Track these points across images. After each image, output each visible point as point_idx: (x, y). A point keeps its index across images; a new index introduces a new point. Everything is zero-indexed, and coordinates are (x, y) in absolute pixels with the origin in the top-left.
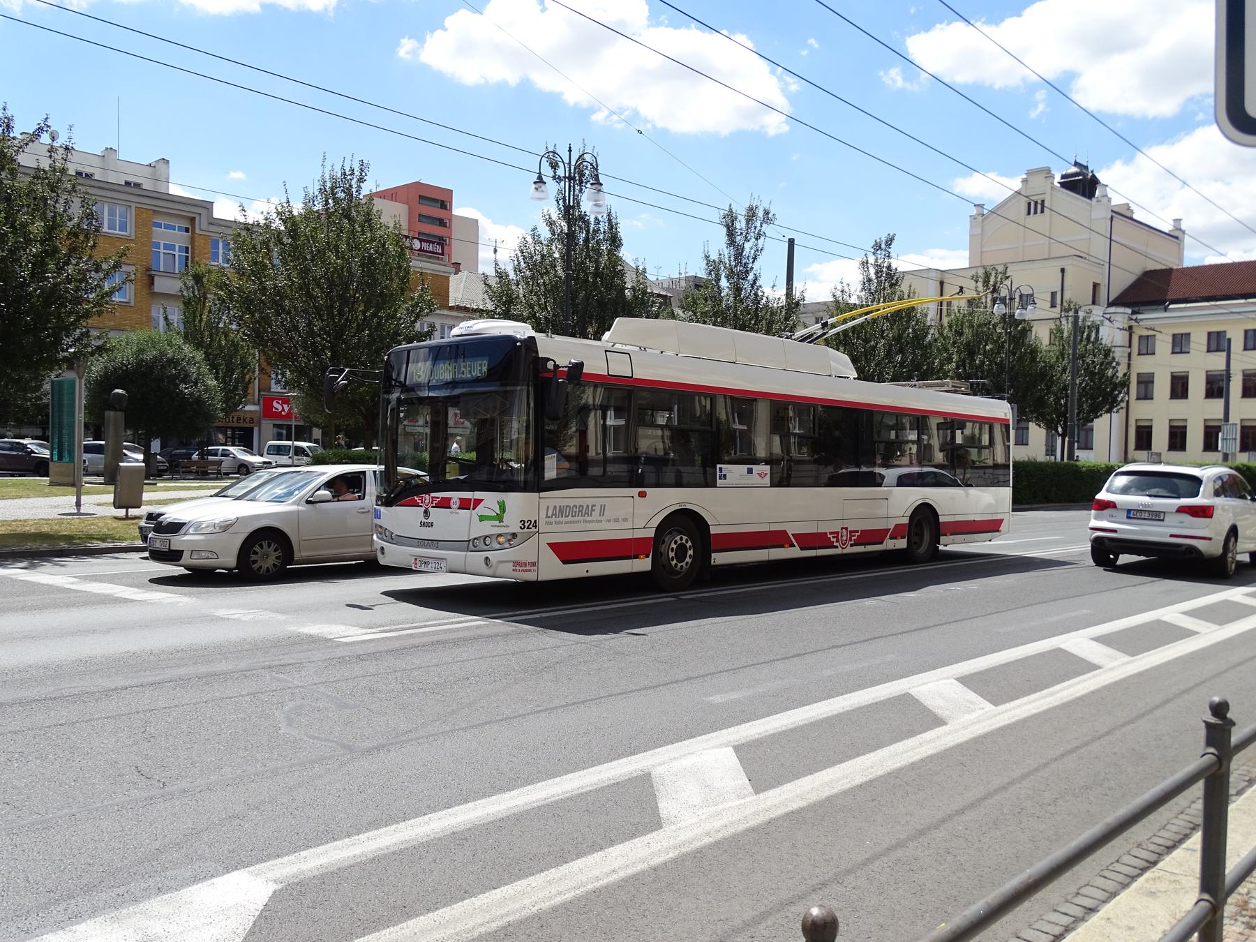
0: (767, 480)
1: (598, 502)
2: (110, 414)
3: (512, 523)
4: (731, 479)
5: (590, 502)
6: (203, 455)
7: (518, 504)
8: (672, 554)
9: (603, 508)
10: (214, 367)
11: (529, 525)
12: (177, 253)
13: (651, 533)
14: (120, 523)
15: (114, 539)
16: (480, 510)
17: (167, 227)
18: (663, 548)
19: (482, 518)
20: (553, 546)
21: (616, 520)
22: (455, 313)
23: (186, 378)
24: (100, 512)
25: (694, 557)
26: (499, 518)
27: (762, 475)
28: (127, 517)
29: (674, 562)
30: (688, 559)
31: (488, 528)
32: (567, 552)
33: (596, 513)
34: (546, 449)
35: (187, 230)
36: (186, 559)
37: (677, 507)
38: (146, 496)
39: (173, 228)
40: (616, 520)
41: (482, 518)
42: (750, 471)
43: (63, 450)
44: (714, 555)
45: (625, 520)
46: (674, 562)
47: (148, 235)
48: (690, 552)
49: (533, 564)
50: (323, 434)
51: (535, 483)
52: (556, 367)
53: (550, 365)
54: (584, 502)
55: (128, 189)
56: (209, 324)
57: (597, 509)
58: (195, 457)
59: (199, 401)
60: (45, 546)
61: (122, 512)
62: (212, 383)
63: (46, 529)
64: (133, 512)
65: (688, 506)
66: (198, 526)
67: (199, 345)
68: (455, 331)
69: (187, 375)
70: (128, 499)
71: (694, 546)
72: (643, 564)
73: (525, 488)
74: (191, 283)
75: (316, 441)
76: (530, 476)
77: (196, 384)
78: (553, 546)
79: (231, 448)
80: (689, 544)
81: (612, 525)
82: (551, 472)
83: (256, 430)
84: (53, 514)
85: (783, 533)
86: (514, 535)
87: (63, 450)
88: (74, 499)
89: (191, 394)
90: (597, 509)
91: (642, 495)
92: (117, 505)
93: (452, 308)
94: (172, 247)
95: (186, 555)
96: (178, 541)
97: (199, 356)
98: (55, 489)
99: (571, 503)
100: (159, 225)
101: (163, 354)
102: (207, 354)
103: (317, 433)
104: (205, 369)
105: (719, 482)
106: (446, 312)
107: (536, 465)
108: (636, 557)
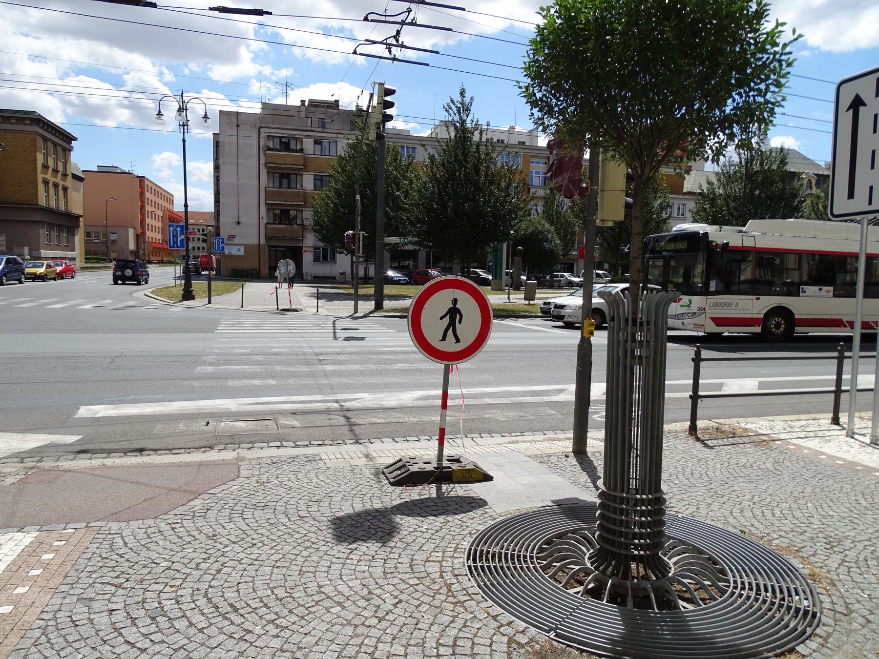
0: (831, 294)
1: (735, 301)
2: (516, 258)
3: (694, 308)
4: (808, 293)
5: (731, 301)
6: (552, 277)
7: (697, 301)
8: (772, 326)
9: (737, 304)
10: (559, 234)
11: (702, 310)
12: (541, 176)
13: (762, 316)
14: (526, 307)
15: (531, 313)
16: (681, 303)
17: (537, 163)
18: (768, 323)
19: (681, 306)
20: (712, 319)
21: (744, 309)
22: (687, 197)
23: (546, 240)
24: (518, 302)
25: (785, 329)
26: (689, 306)
27: (828, 292)
28: (529, 304)
29: (773, 330)
30: (781, 329)
31: (684, 310)
32: (719, 322)
33: (733, 307)
34: (711, 276)
35: (546, 163)
36: (566, 319)
37: (776, 305)
38: (537, 296)
39: (539, 163)
40: (744, 309)
41: (681, 306)
42: (820, 289)
43: (497, 275)
44: (796, 328)
45: (748, 309)
46: (773, 330)
47: (528, 168)
48: (783, 326)
49: (703, 325)
50: (610, 266)
51: (705, 292)
52: (717, 244)
53: (714, 244)
54: (728, 301)
55: (519, 146)
56: (557, 211)
57: (734, 304)
58: (548, 278)
59: (552, 251)
60: (505, 313)
61: (527, 302)
62: (558, 242)
63: (501, 307)
64: (531, 302)
65: (783, 305)
66: (570, 307)
67: (551, 224)
68: (674, 229)
69: (547, 239)
70: (530, 297)
71: (785, 323)
72: (758, 329)
73: (700, 294)
74: (549, 191)
75: (606, 270)
76: (703, 290)
77: (551, 242)
78: (712, 319)
79: (565, 274)
80: (783, 322)
81: (741, 311)
82: (712, 288)
83: (575, 264)
84: (501, 302)
85: (841, 320)
86: (695, 313)
87: (497, 275)
88: (507, 296)
89: (549, 248)
90: (734, 304)
91: (758, 299)
92: (525, 299)
93: (685, 194)
94: (539, 173)
95: (566, 317)
96: (563, 312)
97: (552, 229)
98: (493, 292)
99: (721, 301)
100: (533, 162)
101: (536, 228)
102: (556, 228)
103: (606, 266)
104: (555, 235)
105: (801, 294)
106: (681, 196)
107: (706, 285)
108: (754, 326)
